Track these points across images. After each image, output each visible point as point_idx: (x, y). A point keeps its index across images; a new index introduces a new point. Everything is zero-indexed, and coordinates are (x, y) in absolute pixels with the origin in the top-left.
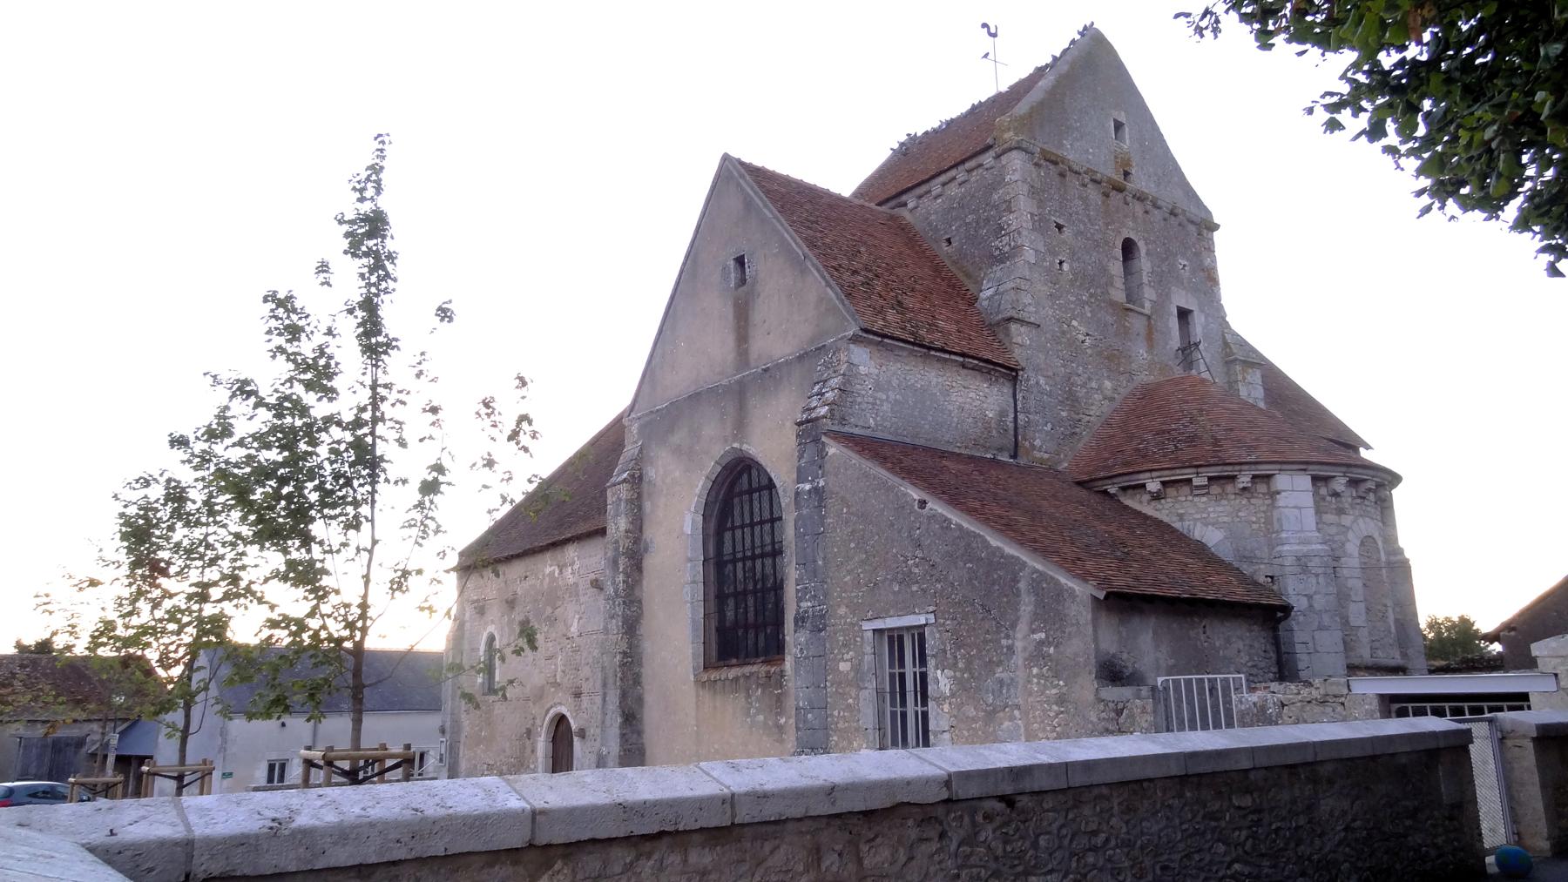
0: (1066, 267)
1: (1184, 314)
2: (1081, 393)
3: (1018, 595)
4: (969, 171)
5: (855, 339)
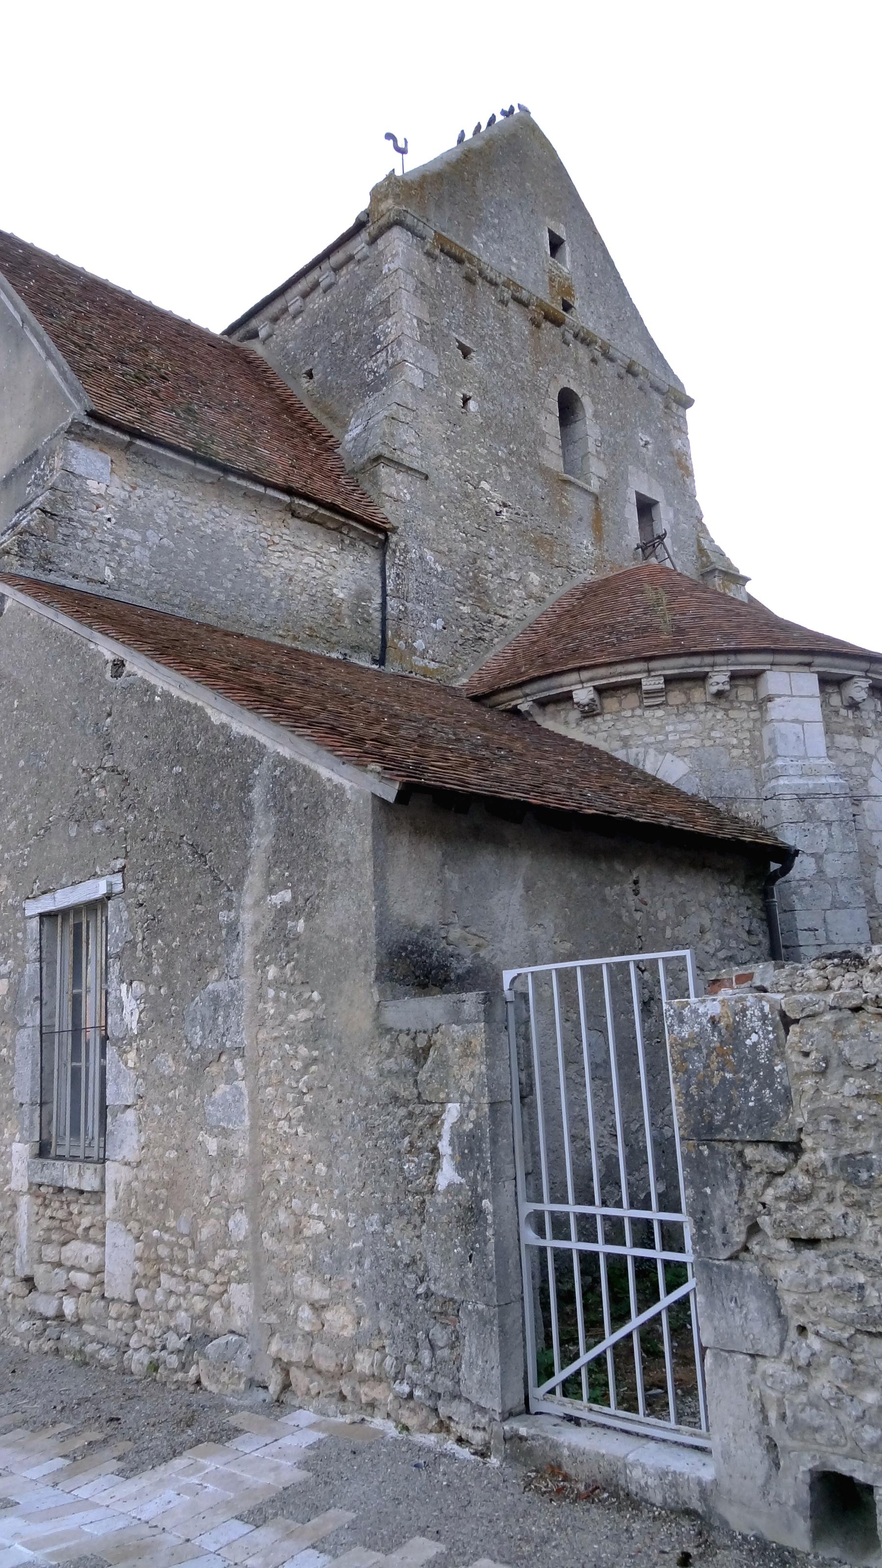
0: (472, 405)
1: (646, 507)
2: (493, 583)
3: (248, 817)
4: (336, 269)
5: (76, 432)
